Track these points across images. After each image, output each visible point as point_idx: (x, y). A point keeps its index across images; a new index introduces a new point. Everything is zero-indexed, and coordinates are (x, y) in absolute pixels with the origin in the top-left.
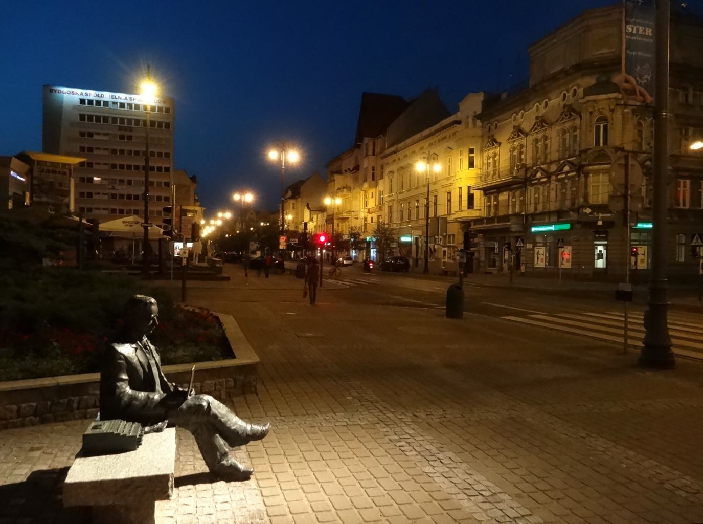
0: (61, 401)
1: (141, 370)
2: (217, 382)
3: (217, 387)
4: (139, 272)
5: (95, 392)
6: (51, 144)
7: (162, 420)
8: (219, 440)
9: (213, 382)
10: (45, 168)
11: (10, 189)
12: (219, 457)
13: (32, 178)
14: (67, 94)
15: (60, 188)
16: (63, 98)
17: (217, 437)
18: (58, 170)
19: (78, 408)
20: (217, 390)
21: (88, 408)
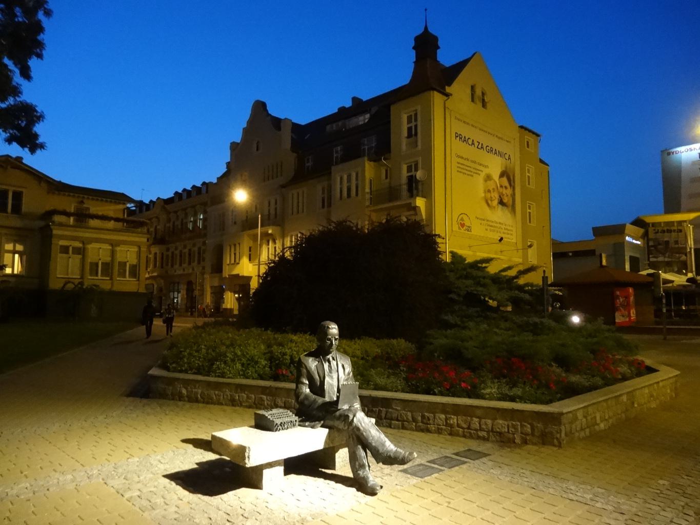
0: (374, 409)
1: (317, 377)
2: (510, 425)
3: (510, 429)
4: (108, 278)
5: (397, 408)
6: (672, 204)
7: (320, 421)
8: (360, 451)
9: (506, 423)
10: (660, 229)
11: (626, 253)
12: (357, 467)
13: (648, 240)
14: (685, 153)
15: (677, 246)
16: (681, 158)
17: (359, 448)
18: (672, 228)
19: (385, 418)
20: (510, 432)
21: (392, 419)
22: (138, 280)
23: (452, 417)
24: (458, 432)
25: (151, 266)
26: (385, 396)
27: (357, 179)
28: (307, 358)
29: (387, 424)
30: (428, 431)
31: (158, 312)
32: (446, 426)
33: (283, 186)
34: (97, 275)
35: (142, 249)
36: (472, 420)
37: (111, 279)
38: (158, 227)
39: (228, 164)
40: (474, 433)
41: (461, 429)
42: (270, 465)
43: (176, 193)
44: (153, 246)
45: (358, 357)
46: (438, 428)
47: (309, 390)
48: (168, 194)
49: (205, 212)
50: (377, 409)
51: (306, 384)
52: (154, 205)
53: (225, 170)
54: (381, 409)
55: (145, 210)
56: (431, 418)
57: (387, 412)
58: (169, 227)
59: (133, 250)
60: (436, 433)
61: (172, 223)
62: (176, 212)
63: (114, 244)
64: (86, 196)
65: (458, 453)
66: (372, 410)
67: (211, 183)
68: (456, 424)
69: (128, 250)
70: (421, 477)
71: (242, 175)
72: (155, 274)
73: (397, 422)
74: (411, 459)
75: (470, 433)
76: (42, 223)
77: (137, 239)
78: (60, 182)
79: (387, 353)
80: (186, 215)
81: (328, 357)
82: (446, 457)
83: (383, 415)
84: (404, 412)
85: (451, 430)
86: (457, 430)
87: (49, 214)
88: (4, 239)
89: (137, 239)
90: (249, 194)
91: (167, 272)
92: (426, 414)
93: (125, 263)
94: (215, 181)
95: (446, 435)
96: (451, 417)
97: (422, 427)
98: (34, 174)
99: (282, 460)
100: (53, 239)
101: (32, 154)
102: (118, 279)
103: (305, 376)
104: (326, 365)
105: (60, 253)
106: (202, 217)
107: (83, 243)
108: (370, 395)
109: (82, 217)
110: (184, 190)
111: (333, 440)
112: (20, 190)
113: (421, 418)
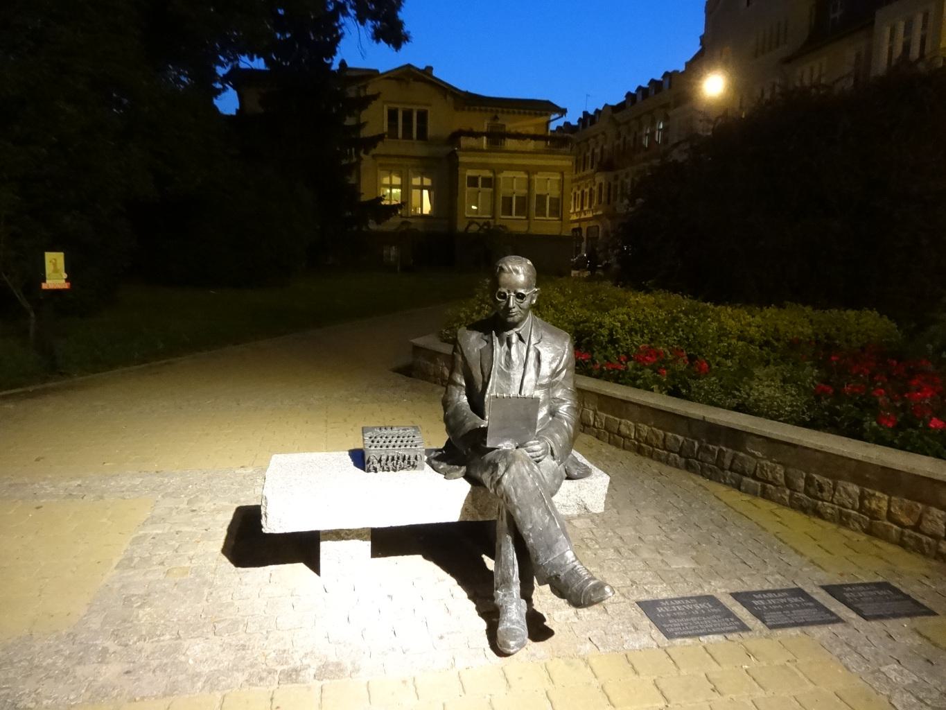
0: (711, 447)
5: (756, 453)
8: (508, 547)
19: (731, 469)
22: (561, 220)
23: (878, 494)
24: (888, 531)
25: (595, 201)
26: (746, 427)
27: (924, 27)
28: (468, 333)
29: (734, 482)
30: (818, 513)
31: (600, 264)
32: (859, 511)
33: (788, 60)
34: (510, 214)
35: (565, 176)
36: (928, 512)
37: (528, 218)
38: (605, 147)
39: (702, 39)
40: (928, 544)
41: (895, 527)
42: (338, 535)
43: (629, 95)
44: (598, 173)
45: (752, 341)
46: (840, 511)
47: (465, 398)
48: (617, 98)
49: (666, 119)
50: (717, 448)
51: (462, 386)
52: (600, 114)
53: (699, 48)
54: (724, 449)
55: (589, 123)
56: (826, 488)
57: (734, 457)
58: (619, 146)
59: (553, 178)
60: (834, 522)
61: (622, 139)
62: (627, 123)
63: (530, 171)
64: (500, 109)
65: (841, 587)
66: (707, 449)
67: (676, 72)
68: (884, 513)
69: (548, 179)
70: (669, 636)
71: (721, 54)
72: (600, 213)
73: (753, 481)
74: (594, 600)
75: (919, 541)
76: (448, 149)
77: (559, 163)
78: (467, 93)
79: (828, 337)
80: (641, 128)
82: (799, 592)
83: (727, 462)
84: (769, 463)
85: (871, 523)
86: (885, 526)
87: (455, 137)
88: (411, 173)
89: (559, 163)
90: (700, 77)
91: (615, 209)
93: (545, 196)
94: (682, 68)
95: (856, 530)
96: (874, 495)
97: (805, 503)
98: (440, 86)
99: (367, 528)
100: (459, 169)
101: (396, 51)
102: (502, 217)
103: (461, 371)
104: (499, 350)
105: (469, 186)
106: (661, 126)
107: (494, 173)
108: (704, 417)
109: (497, 137)
110: (640, 88)
111: (486, 508)
112: (424, 108)
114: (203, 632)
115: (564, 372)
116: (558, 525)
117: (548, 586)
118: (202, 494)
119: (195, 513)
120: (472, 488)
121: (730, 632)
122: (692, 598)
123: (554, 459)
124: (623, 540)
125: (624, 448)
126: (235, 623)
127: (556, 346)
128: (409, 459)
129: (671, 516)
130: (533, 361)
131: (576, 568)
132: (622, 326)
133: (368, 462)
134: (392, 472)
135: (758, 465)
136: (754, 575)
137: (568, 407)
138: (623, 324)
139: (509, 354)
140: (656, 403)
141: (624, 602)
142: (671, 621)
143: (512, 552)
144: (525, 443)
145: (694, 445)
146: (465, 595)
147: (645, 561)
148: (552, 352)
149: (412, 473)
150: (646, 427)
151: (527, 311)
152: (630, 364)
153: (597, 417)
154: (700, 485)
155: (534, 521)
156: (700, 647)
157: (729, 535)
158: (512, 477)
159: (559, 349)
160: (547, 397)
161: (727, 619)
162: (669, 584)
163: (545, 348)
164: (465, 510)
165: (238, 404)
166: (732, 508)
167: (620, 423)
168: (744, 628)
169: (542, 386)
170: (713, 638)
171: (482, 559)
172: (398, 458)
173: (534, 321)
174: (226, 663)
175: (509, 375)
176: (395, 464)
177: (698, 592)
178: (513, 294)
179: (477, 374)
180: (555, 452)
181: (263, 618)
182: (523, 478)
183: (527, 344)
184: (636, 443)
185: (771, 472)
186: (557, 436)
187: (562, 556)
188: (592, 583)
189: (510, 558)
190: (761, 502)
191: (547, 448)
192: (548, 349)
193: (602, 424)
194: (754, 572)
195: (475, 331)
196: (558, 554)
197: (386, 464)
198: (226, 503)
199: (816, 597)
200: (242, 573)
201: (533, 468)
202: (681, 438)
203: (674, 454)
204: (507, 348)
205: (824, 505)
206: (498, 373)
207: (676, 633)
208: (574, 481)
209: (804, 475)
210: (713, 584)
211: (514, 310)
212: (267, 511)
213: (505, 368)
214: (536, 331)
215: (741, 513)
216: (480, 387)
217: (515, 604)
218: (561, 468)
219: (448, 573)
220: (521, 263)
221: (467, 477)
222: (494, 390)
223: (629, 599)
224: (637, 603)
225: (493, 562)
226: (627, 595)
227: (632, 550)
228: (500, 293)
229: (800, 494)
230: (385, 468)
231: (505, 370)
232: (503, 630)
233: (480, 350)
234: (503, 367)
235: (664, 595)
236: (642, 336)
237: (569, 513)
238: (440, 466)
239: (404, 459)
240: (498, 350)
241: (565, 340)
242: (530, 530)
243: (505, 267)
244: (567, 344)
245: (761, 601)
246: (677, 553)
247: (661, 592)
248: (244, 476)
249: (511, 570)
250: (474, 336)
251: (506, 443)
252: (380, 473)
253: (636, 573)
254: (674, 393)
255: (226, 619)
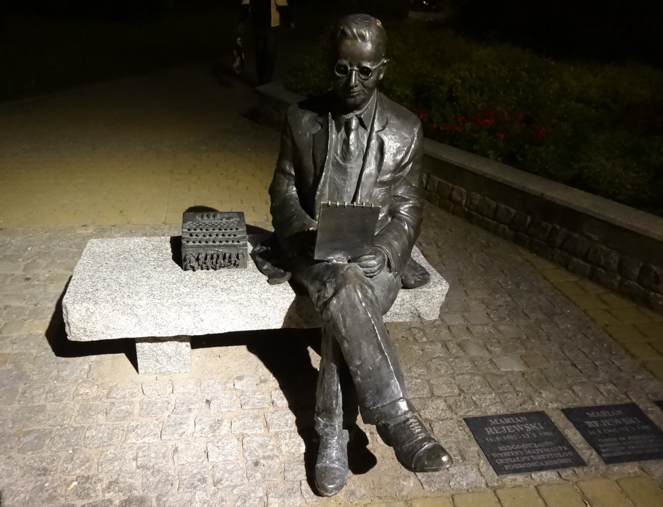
0: (544, 223)
8: (333, 376)
19: (560, 248)
28: (300, 112)
47: (294, 189)
50: (550, 226)
51: (291, 175)
54: (558, 227)
70: (499, 470)
81: (347, 117)
82: (632, 410)
83: (559, 241)
84: (604, 248)
92: (654, 268)
104: (335, 136)
108: (542, 194)
113: (640, 273)
114: (6, 448)
115: (410, 166)
116: (391, 367)
117: (375, 426)
118: (40, 258)
119: (28, 282)
120: (296, 298)
121: (564, 466)
122: (522, 414)
123: (390, 272)
124: (451, 332)
125: (453, 213)
126: (42, 436)
127: (404, 134)
128: (230, 257)
129: (501, 300)
130: (374, 153)
131: (409, 423)
132: (462, 83)
133: (185, 260)
134: (211, 270)
135: (592, 248)
136: (585, 383)
137: (411, 207)
138: (463, 80)
139: (346, 142)
140: (493, 174)
141: (451, 419)
142: (500, 449)
143: (336, 382)
144: (360, 257)
145: (526, 219)
146: (285, 402)
147: (472, 361)
148: (397, 142)
149: (235, 273)
150: (478, 196)
151: (371, 90)
152: (468, 126)
153: (430, 180)
154: (527, 261)
155: (362, 358)
156: (532, 487)
157: (558, 328)
158: (342, 303)
159: (406, 138)
160: (387, 196)
161: (560, 448)
162: (498, 394)
163: (390, 136)
164: (289, 318)
165: (94, 149)
166: (560, 291)
167: (453, 189)
168: (579, 462)
169: (383, 184)
170: (546, 475)
171: (307, 352)
172: (218, 256)
173: (379, 100)
174: (23, 495)
175: (346, 169)
176: (214, 263)
177: (529, 407)
178: (356, 68)
179: (309, 163)
180: (393, 264)
181: (72, 429)
182: (353, 306)
183: (369, 131)
184: (467, 210)
185: (604, 256)
186: (395, 243)
187: (394, 404)
188: (427, 446)
189: (334, 388)
190: (590, 286)
191: (384, 260)
192: (393, 137)
193: (434, 188)
194: (585, 380)
195: (308, 111)
196: (388, 402)
197: (205, 263)
198: (61, 271)
199: (651, 417)
200: (62, 363)
201: (367, 292)
202: (513, 211)
203: (503, 226)
204: (344, 135)
205: (656, 296)
206: (333, 165)
207: (506, 467)
208: (411, 290)
209: (641, 264)
210: (544, 395)
211: (356, 89)
212: (69, 321)
213: (341, 158)
214: (381, 114)
215: (568, 297)
216: (311, 180)
217: (336, 438)
218: (398, 279)
219: (271, 372)
220: (368, 26)
221: (296, 285)
222: (327, 186)
223: (457, 414)
224: (465, 419)
225: (319, 358)
226: (454, 408)
227: (459, 345)
228: (341, 65)
229: (632, 282)
230: (204, 266)
231: (341, 162)
232: (322, 467)
233: (314, 135)
234: (338, 158)
235: (493, 410)
236: (481, 95)
237: (401, 321)
238: (264, 265)
239: (224, 258)
240: (334, 136)
241: (415, 125)
242: (358, 367)
243: (349, 32)
244: (416, 130)
245: (595, 422)
246: (505, 350)
247: (490, 405)
248: (84, 238)
249: (334, 402)
250: (307, 118)
251: (337, 256)
252: (199, 272)
253: (464, 378)
254: (509, 159)
255: (32, 431)
